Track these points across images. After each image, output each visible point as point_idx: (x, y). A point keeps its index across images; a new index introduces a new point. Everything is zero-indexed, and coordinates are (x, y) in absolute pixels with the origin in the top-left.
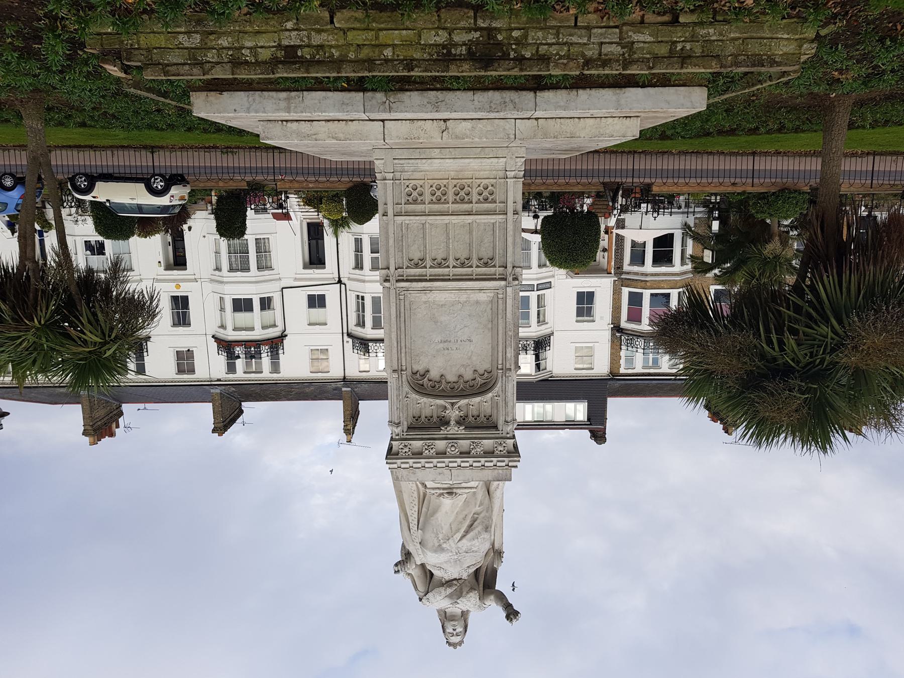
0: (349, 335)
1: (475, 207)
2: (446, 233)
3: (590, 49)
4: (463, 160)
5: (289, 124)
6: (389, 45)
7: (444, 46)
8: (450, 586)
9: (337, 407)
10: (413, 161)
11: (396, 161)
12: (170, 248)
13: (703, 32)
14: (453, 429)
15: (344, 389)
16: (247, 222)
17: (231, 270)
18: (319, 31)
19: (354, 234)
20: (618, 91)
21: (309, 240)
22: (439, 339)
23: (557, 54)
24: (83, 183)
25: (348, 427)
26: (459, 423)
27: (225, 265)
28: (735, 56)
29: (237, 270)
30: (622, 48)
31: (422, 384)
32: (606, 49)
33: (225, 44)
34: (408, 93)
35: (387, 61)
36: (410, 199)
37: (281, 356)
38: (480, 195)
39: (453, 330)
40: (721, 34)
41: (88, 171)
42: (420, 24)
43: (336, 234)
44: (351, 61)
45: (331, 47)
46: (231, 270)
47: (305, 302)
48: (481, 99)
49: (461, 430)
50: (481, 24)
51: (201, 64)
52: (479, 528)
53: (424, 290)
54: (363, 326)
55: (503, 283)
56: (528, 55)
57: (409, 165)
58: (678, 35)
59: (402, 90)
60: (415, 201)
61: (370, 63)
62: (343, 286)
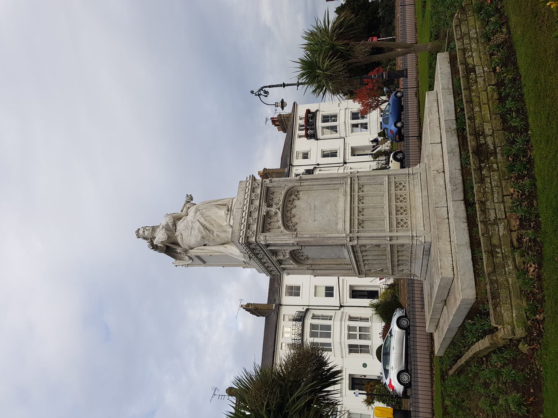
0: (307, 310)
1: (394, 204)
2: (378, 201)
3: (491, 204)
4: (421, 207)
5: (436, 103)
6: (481, 109)
7: (483, 133)
8: (173, 225)
9: (263, 299)
10: (419, 182)
11: (419, 174)
13: (510, 262)
14: (264, 209)
15: (274, 305)
18: (484, 80)
19: (372, 317)
20: (469, 245)
22: (317, 204)
23: (486, 187)
24: (399, 156)
25: (250, 306)
26: (268, 213)
30: (494, 220)
31: (291, 195)
32: (492, 212)
33: (473, 46)
34: (457, 139)
35: (473, 109)
36: (399, 209)
38: (401, 220)
39: (322, 217)
40: (510, 273)
41: (406, 158)
42: (494, 122)
43: (372, 306)
44: (470, 94)
45: (477, 86)
47: (329, 284)
48: (457, 173)
49: (264, 213)
50: (498, 150)
51: (462, 38)
53: (345, 192)
54: (312, 318)
55: (348, 232)
56: (483, 172)
57: (417, 181)
58: (506, 249)
59: (458, 136)
60: (396, 187)
62: (338, 308)
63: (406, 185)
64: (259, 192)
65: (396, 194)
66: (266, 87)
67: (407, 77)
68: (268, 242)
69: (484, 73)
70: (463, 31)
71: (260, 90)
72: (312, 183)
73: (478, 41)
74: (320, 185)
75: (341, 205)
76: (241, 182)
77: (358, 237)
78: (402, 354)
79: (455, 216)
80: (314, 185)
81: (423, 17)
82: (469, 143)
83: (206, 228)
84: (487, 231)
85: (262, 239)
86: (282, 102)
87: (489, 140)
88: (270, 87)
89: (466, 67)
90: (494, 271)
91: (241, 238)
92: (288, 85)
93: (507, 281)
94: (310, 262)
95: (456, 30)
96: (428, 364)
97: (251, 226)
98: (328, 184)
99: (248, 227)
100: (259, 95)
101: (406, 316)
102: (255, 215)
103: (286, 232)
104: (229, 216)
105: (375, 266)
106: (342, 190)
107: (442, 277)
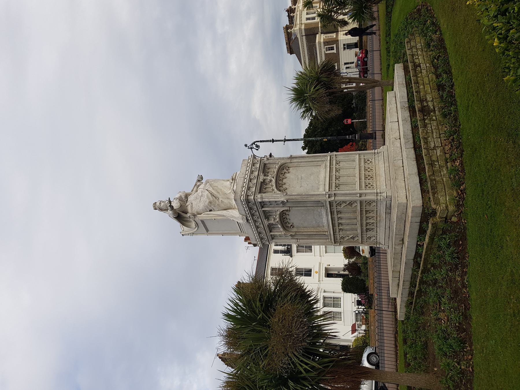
1: (363, 172)
5: (394, 99)
7: (426, 100)
12: (337, 273)
13: (444, 169)
17: (324, 298)
20: (417, 174)
22: (303, 176)
24: (374, 359)
26: (264, 180)
27: (326, 295)
28: (435, 180)
29: (324, 301)
35: (419, 87)
37: (281, 254)
40: (444, 175)
46: (324, 298)
49: (261, 180)
52: (211, 199)
58: (442, 163)
60: (365, 162)
61: (417, 83)
64: (258, 166)
66: (258, 141)
67: (375, 139)
68: (263, 200)
71: (252, 144)
72: (300, 161)
75: (322, 176)
76: (244, 160)
77: (335, 194)
80: (301, 162)
81: (388, 76)
84: (428, 153)
85: (259, 198)
86: (271, 155)
87: (430, 104)
88: (261, 141)
92: (276, 141)
93: (443, 180)
94: (295, 230)
96: (393, 342)
97: (251, 188)
99: (249, 188)
100: (251, 148)
101: (375, 353)
106: (323, 166)
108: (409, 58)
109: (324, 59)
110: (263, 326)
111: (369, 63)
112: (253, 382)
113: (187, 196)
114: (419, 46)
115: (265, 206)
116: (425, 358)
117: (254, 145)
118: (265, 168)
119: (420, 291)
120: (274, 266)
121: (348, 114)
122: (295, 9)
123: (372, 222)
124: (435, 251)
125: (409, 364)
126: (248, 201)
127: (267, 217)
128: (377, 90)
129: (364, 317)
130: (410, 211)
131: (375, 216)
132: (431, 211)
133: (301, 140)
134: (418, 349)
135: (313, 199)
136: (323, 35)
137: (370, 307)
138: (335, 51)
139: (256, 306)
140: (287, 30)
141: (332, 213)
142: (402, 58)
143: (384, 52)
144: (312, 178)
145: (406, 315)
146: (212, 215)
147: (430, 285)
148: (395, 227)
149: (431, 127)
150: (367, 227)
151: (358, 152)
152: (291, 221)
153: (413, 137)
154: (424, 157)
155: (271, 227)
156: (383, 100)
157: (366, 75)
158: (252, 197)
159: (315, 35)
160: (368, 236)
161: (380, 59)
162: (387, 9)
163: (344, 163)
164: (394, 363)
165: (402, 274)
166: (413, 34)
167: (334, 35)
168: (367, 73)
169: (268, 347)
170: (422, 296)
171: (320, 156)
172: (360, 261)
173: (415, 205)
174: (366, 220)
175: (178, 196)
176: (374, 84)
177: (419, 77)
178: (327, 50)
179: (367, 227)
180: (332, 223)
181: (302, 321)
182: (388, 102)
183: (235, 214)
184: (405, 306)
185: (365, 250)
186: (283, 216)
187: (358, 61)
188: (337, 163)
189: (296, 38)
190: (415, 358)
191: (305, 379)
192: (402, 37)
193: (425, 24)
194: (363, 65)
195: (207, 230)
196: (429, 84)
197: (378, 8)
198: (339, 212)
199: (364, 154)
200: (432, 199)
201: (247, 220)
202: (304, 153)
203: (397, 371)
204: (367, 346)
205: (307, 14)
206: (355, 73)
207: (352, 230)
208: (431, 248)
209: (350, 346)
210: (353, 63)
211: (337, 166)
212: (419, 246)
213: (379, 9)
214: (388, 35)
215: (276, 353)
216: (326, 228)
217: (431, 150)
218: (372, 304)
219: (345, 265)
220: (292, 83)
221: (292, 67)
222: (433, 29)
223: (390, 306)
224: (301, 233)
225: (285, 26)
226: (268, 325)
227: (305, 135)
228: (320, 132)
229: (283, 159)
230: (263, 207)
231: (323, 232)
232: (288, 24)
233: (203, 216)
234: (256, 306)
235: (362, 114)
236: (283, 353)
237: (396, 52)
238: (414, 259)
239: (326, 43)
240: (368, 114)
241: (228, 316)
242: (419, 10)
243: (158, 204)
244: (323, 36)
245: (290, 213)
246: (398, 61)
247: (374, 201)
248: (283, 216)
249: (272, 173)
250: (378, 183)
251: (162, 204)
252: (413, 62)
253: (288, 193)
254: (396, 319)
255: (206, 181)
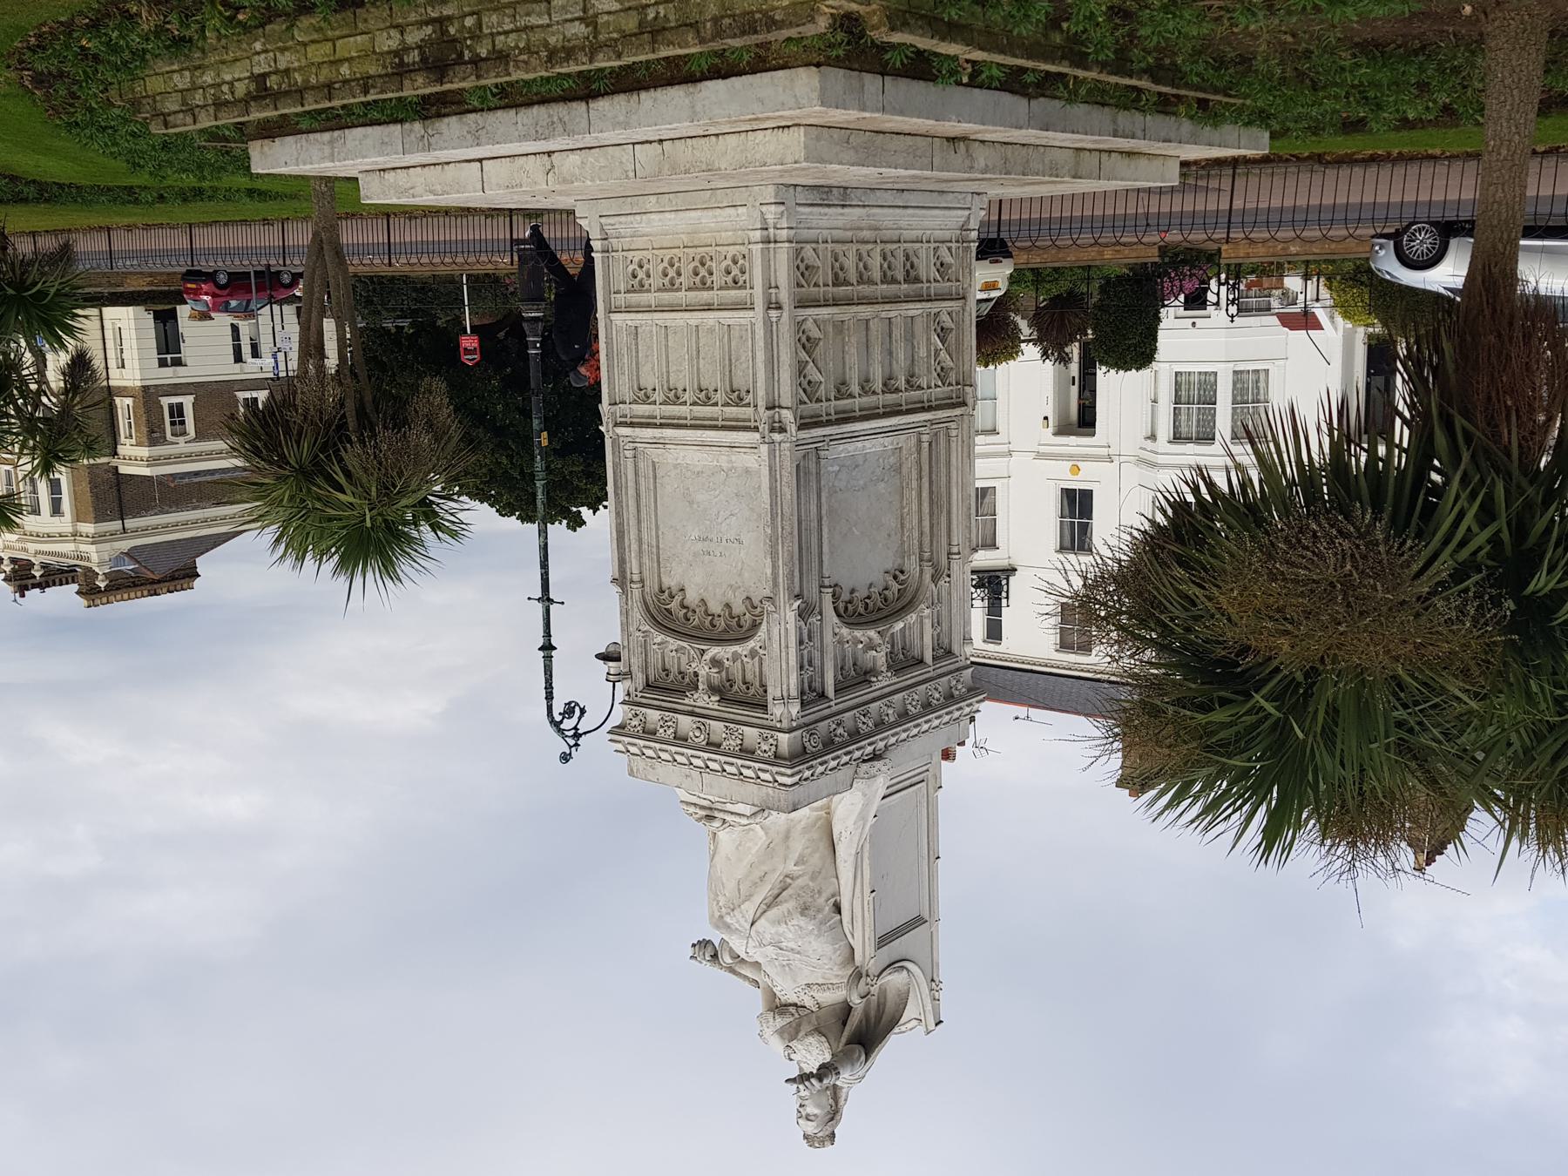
1: (682, 297)
5: (390, 176)
6: (346, 60)
7: (396, 53)
8: (781, 1014)
10: (623, 219)
11: (603, 220)
12: (1075, 390)
16: (1160, 333)
17: (1177, 438)
18: (283, 50)
20: (690, 88)
21: (1369, 375)
22: (695, 534)
23: (517, 47)
24: (1422, 242)
26: (713, 689)
27: (1165, 430)
28: (716, 20)
29: (1189, 439)
33: (210, 81)
34: (446, 120)
35: (345, 82)
41: (1436, 215)
42: (372, 24)
44: (313, 88)
46: (1177, 438)
52: (791, 905)
55: (757, 435)
59: (440, 116)
61: (328, 89)
63: (636, 260)
64: (653, 715)
65: (659, 290)
68: (794, 693)
69: (266, 51)
70: (177, 108)
71: (561, 731)
72: (634, 547)
73: (200, 67)
74: (639, 522)
78: (1543, 250)
79: (626, 125)
80: (640, 541)
81: (293, 197)
82: (420, 92)
83: (774, 901)
84: (610, 45)
85: (784, 711)
86: (605, 657)
87: (414, 37)
88: (549, 696)
89: (255, 98)
90: (694, 26)
91: (781, 779)
94: (912, 565)
95: (175, 126)
96: (1358, 171)
97: (747, 743)
98: (638, 495)
99: (746, 752)
100: (577, 736)
101: (1396, 236)
102: (717, 727)
103: (762, 632)
104: (729, 818)
105: (923, 353)
106: (654, 453)
107: (806, 160)
108: (228, 119)
109: (220, 445)
110: (1307, 695)
111: (237, 266)
112: (1538, 737)
113: (778, 1007)
114: (182, 81)
115: (817, 685)
116: (1423, 48)
117: (566, 721)
118: (665, 687)
119: (1154, 73)
120: (1053, 638)
121: (436, 348)
122: (13, 561)
123: (879, 259)
124: (996, 17)
125: (1446, 109)
126: (800, 757)
127: (864, 676)
128: (350, 235)
129: (1252, 283)
130: (838, 116)
131: (855, 247)
132: (840, 36)
133: (543, 533)
134: (1384, 76)
135: (788, 492)
136: (120, 449)
137: (1212, 258)
138: (188, 401)
139: (1231, 724)
140: (98, 591)
141: (845, 418)
142: (228, 149)
143: (196, 211)
144: (703, 493)
145: (1248, 124)
146: (857, 903)
147: (1132, 35)
148: (902, 172)
149: (506, 33)
150: (900, 277)
151: (600, 314)
152: (879, 579)
153: (543, 101)
154: (627, 60)
155: (905, 661)
156: (387, 214)
157: (286, 279)
158: (784, 738)
159: (119, 480)
160: (934, 273)
161: (226, 224)
162: (25, 201)
163: (645, 370)
164: (1441, 169)
165: (1087, 141)
166: (136, 104)
167: (123, 403)
168: (279, 272)
169: (1394, 677)
170: (1174, 64)
171: (616, 466)
172: (1029, 298)
173: (815, 95)
174: (871, 282)
175: (777, 1045)
176: (326, 247)
177: (307, 81)
178: (184, 433)
179: (900, 277)
180: (886, 415)
181: (1286, 540)
182: (403, 201)
183: (853, 805)
184: (1215, 126)
185: (990, 278)
186: (856, 613)
187: (227, 310)
188: (646, 400)
189: (131, 554)
190: (1423, 87)
191: (1520, 529)
192: (142, 145)
193: (96, 58)
194: (246, 287)
195: (918, 921)
196: (333, 41)
197: (23, 233)
198: (842, 391)
199: (608, 292)
200: (793, 32)
201: (875, 757)
202: (598, 522)
203: (1476, 156)
204: (1370, 270)
205: (36, 511)
206: (277, 318)
207: (910, 337)
208: (988, 31)
209: (1370, 337)
210: (235, 329)
211: (658, 397)
212: (977, 78)
213: (30, 233)
214: (129, 196)
215: (1417, 647)
216: (906, 442)
217: (596, 33)
218: (1200, 251)
219: (1045, 355)
220: (319, 578)
221: (249, 568)
222: (118, 27)
223: (1214, 184)
224: (927, 540)
225: (83, 602)
226: (1307, 675)
227: (522, 519)
228: (510, 457)
229: (626, 613)
230: (822, 695)
231: (919, 452)
232: (75, 587)
233: (862, 941)
234: (1231, 724)
235: (440, 291)
236: (1417, 615)
237: (199, 167)
238: (1029, 97)
239: (154, 435)
240: (442, 270)
241: (1271, 836)
242: (39, 79)
243: (811, 1128)
244: (127, 448)
245: (847, 586)
246: (236, 159)
247: (798, 252)
248: (856, 613)
249: (684, 659)
250: (727, 236)
251: (811, 1109)
252: (246, 102)
253: (767, 592)
254: (1265, 160)
255: (717, 927)
